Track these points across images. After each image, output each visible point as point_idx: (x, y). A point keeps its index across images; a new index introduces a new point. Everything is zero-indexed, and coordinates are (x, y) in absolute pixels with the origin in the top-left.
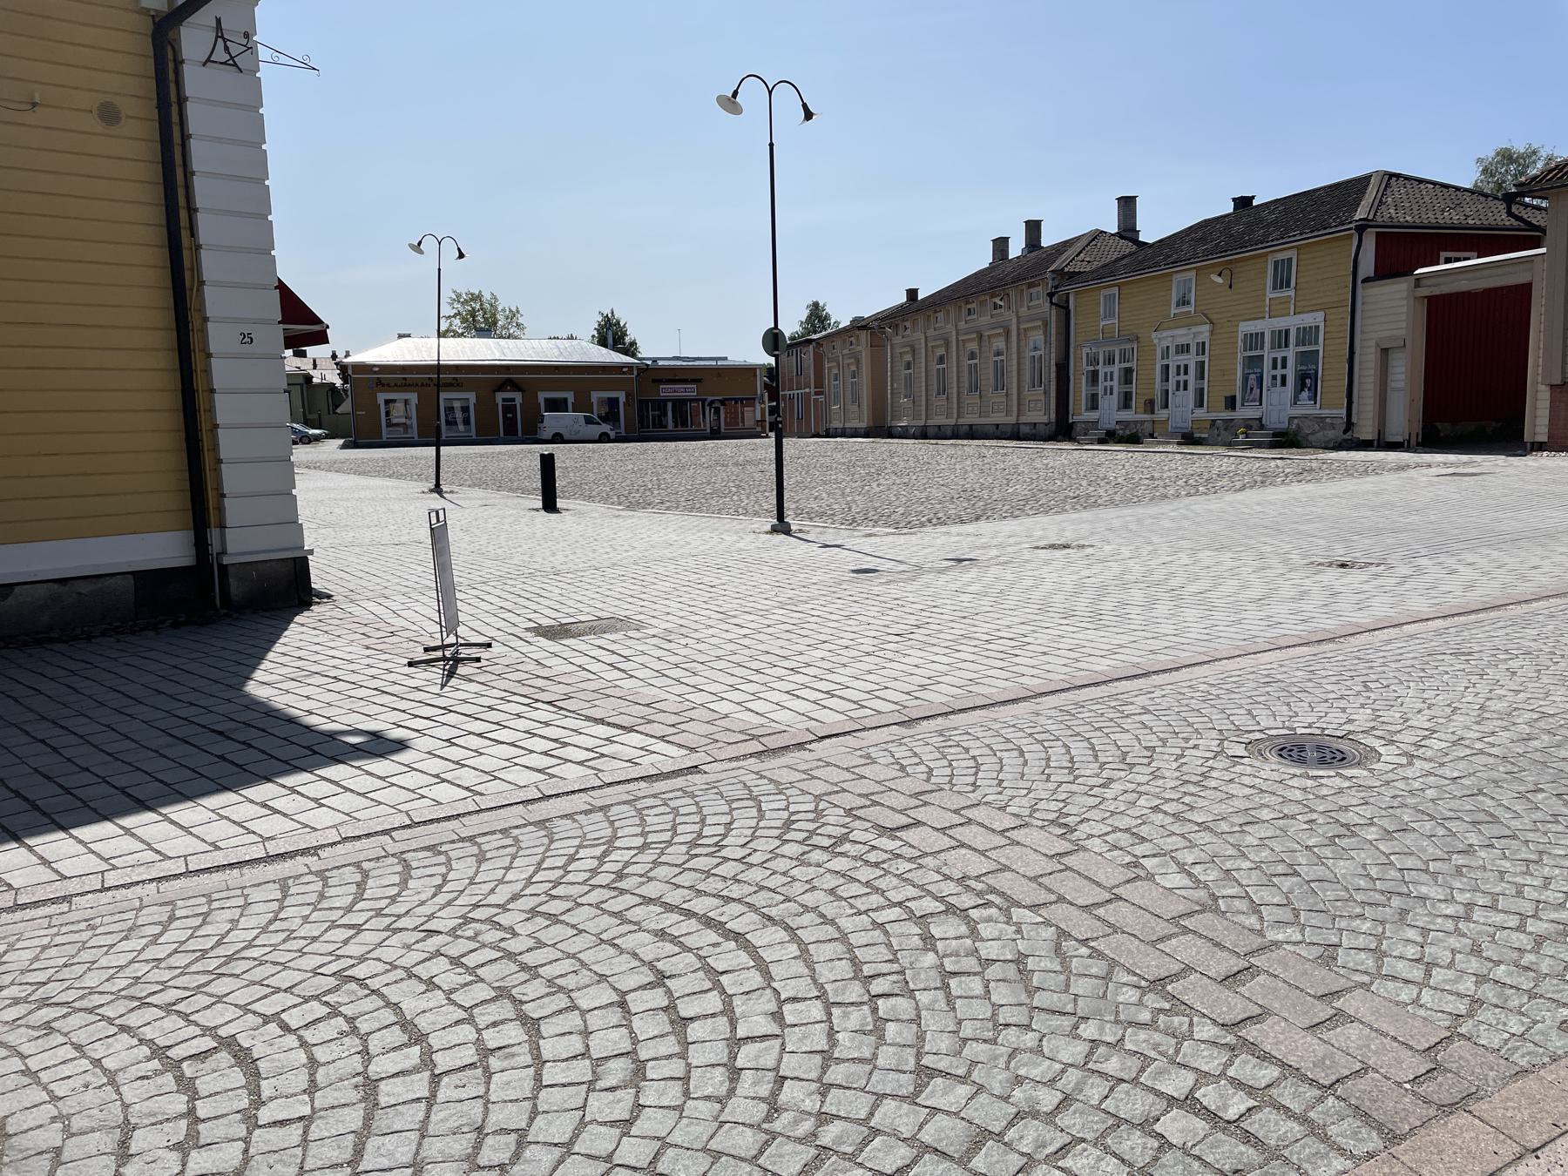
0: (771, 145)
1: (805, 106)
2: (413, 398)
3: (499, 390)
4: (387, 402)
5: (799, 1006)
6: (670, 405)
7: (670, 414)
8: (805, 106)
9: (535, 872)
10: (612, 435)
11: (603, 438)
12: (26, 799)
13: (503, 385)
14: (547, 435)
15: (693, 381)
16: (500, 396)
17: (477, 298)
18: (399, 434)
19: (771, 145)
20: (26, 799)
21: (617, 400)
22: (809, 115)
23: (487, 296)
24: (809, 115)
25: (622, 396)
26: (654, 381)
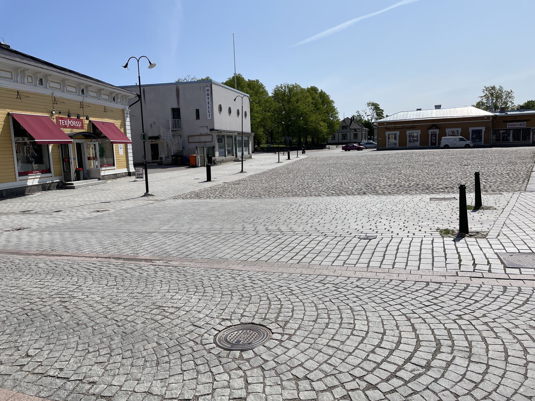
0: (139, 77)
1: (127, 64)
2: (398, 133)
3: (430, 129)
4: (389, 134)
5: (220, 376)
6: (511, 132)
7: (511, 135)
8: (127, 64)
9: (463, 308)
10: (471, 145)
11: (467, 146)
12: (503, 246)
13: (431, 127)
14: (442, 145)
15: (524, 121)
16: (430, 131)
17: (493, 88)
18: (412, 144)
19: (139, 77)
20: (503, 246)
21: (482, 130)
22: (126, 66)
23: (497, 87)
24: (126, 66)
25: (483, 129)
26: (504, 121)
